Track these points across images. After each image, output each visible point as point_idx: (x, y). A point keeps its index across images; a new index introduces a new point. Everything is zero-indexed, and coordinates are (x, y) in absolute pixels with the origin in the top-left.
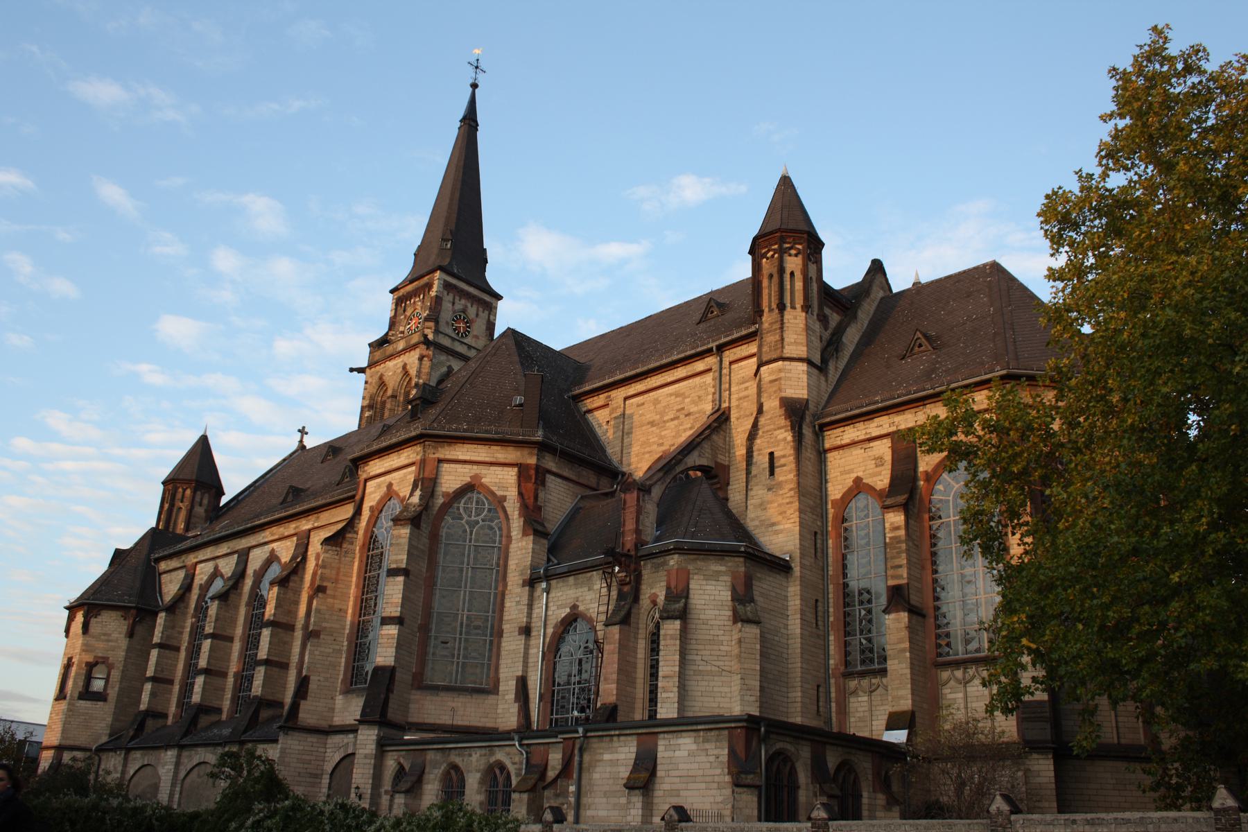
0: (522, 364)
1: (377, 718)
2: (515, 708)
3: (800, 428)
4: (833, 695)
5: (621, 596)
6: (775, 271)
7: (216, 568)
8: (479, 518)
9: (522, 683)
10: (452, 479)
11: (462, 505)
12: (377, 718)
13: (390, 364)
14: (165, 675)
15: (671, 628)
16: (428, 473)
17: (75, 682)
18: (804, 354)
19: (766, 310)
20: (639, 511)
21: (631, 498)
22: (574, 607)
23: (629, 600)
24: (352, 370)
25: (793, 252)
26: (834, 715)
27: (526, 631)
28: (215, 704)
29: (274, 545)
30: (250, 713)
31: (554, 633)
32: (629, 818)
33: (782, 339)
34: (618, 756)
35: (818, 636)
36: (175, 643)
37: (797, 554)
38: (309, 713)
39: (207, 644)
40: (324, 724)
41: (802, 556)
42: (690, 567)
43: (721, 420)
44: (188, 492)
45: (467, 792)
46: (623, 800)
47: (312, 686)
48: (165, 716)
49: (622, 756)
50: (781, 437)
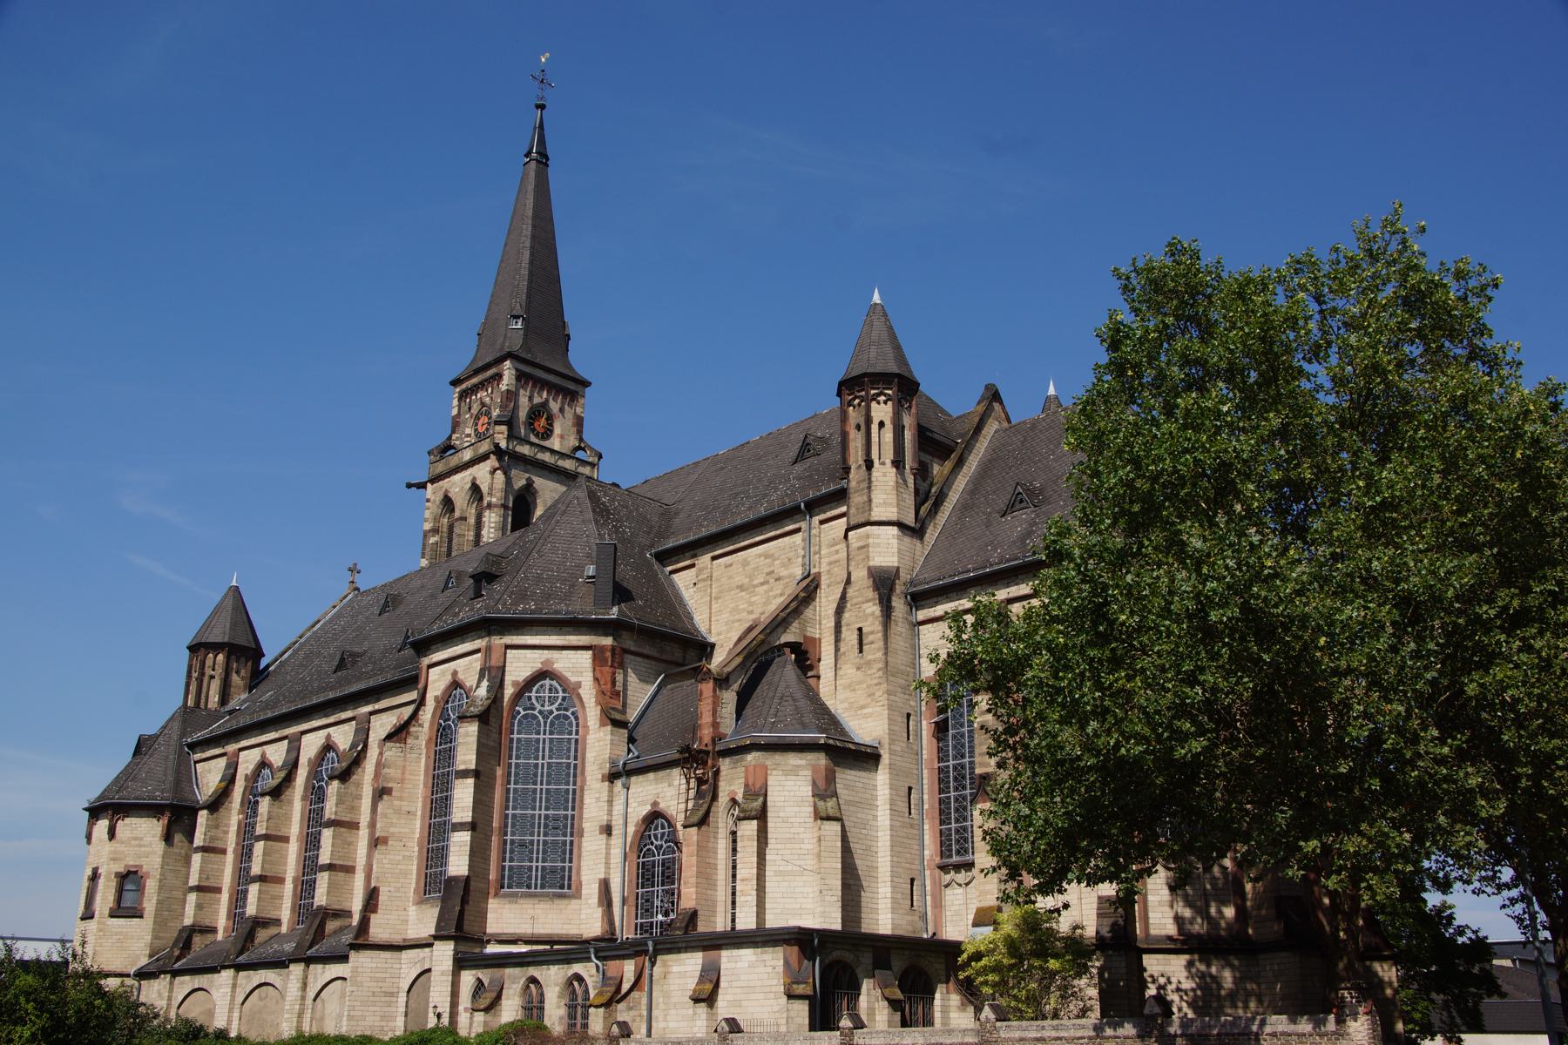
0: (596, 522)
1: (452, 932)
2: (598, 913)
3: (889, 600)
4: (928, 888)
5: (699, 795)
6: (862, 421)
7: (263, 755)
8: (553, 708)
9: (605, 886)
10: (520, 666)
11: (533, 694)
12: (452, 932)
13: (457, 477)
14: (212, 883)
15: (749, 828)
16: (495, 661)
17: (104, 899)
18: (894, 517)
19: (853, 467)
20: (716, 703)
21: (707, 688)
22: (655, 804)
23: (708, 799)
24: (409, 486)
25: (882, 398)
26: (929, 908)
27: (608, 830)
28: (273, 914)
29: (330, 730)
30: (315, 926)
31: (636, 832)
32: (695, 1030)
33: (870, 501)
34: (683, 969)
35: (912, 826)
36: (219, 844)
37: (886, 741)
38: (380, 929)
39: (259, 847)
40: (396, 939)
41: (892, 742)
42: (768, 763)
43: (809, 591)
44: (220, 657)
45: (547, 1006)
46: (691, 1011)
47: (383, 898)
48: (214, 930)
49: (689, 968)
50: (869, 611)
